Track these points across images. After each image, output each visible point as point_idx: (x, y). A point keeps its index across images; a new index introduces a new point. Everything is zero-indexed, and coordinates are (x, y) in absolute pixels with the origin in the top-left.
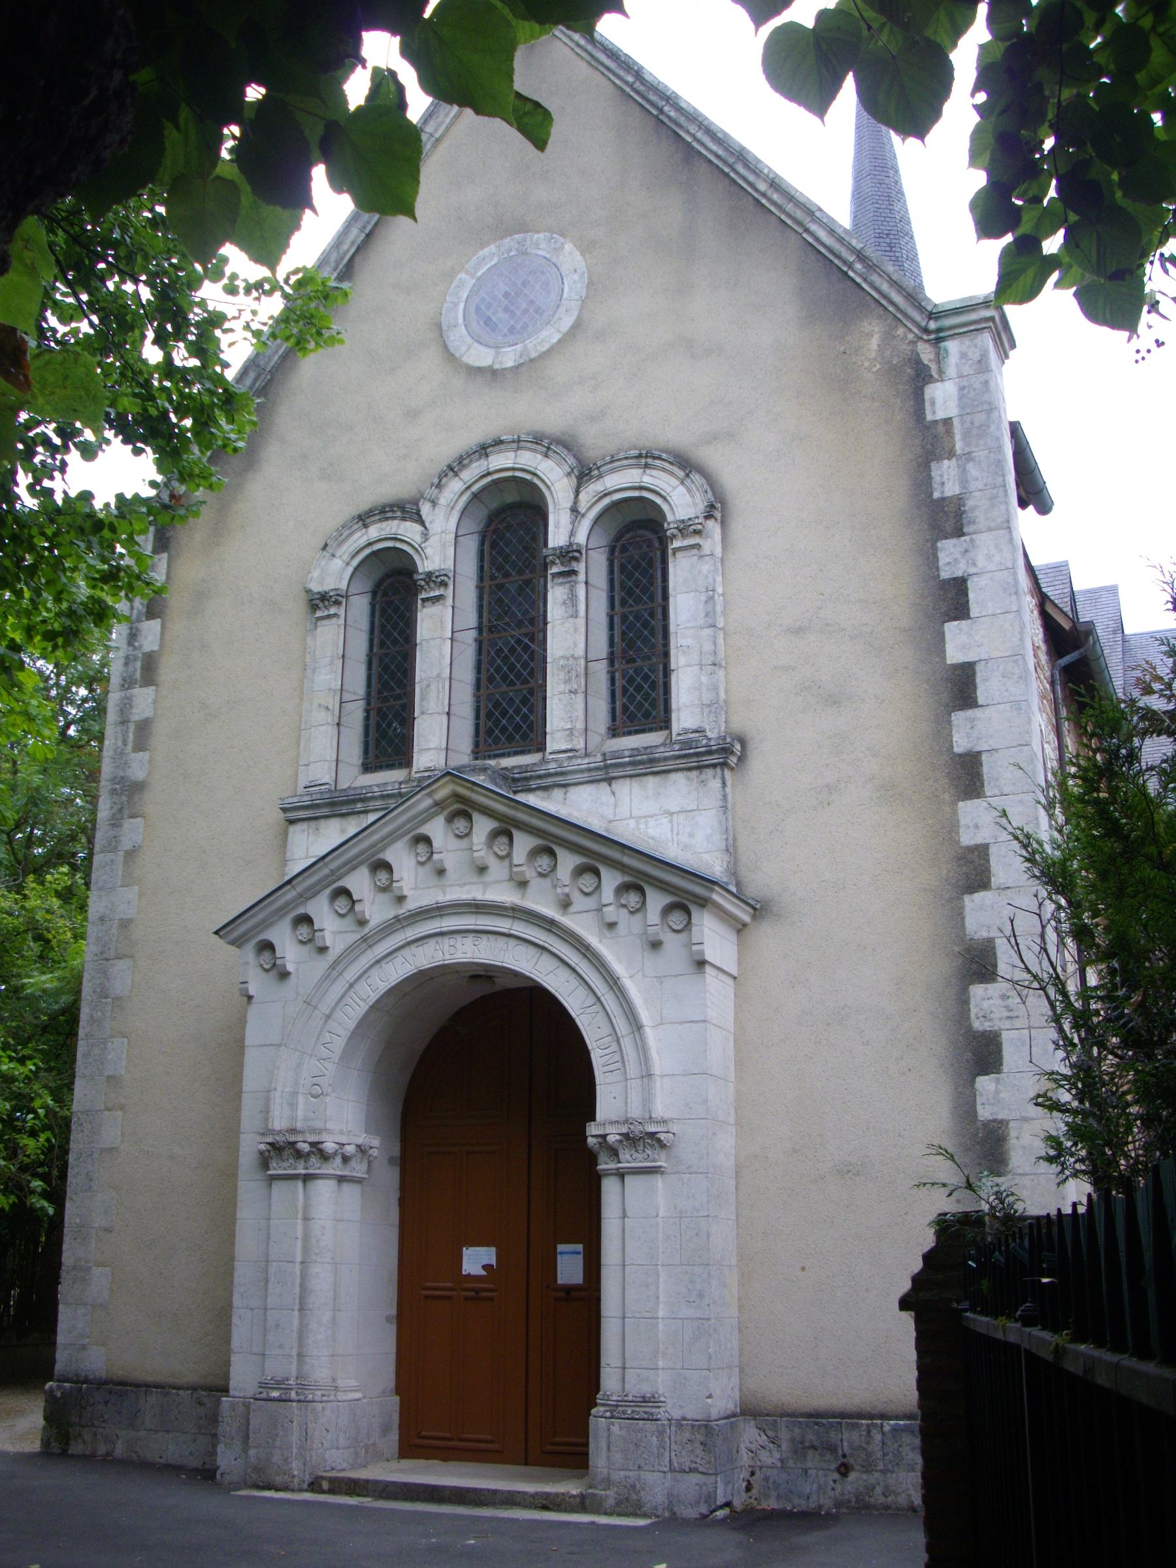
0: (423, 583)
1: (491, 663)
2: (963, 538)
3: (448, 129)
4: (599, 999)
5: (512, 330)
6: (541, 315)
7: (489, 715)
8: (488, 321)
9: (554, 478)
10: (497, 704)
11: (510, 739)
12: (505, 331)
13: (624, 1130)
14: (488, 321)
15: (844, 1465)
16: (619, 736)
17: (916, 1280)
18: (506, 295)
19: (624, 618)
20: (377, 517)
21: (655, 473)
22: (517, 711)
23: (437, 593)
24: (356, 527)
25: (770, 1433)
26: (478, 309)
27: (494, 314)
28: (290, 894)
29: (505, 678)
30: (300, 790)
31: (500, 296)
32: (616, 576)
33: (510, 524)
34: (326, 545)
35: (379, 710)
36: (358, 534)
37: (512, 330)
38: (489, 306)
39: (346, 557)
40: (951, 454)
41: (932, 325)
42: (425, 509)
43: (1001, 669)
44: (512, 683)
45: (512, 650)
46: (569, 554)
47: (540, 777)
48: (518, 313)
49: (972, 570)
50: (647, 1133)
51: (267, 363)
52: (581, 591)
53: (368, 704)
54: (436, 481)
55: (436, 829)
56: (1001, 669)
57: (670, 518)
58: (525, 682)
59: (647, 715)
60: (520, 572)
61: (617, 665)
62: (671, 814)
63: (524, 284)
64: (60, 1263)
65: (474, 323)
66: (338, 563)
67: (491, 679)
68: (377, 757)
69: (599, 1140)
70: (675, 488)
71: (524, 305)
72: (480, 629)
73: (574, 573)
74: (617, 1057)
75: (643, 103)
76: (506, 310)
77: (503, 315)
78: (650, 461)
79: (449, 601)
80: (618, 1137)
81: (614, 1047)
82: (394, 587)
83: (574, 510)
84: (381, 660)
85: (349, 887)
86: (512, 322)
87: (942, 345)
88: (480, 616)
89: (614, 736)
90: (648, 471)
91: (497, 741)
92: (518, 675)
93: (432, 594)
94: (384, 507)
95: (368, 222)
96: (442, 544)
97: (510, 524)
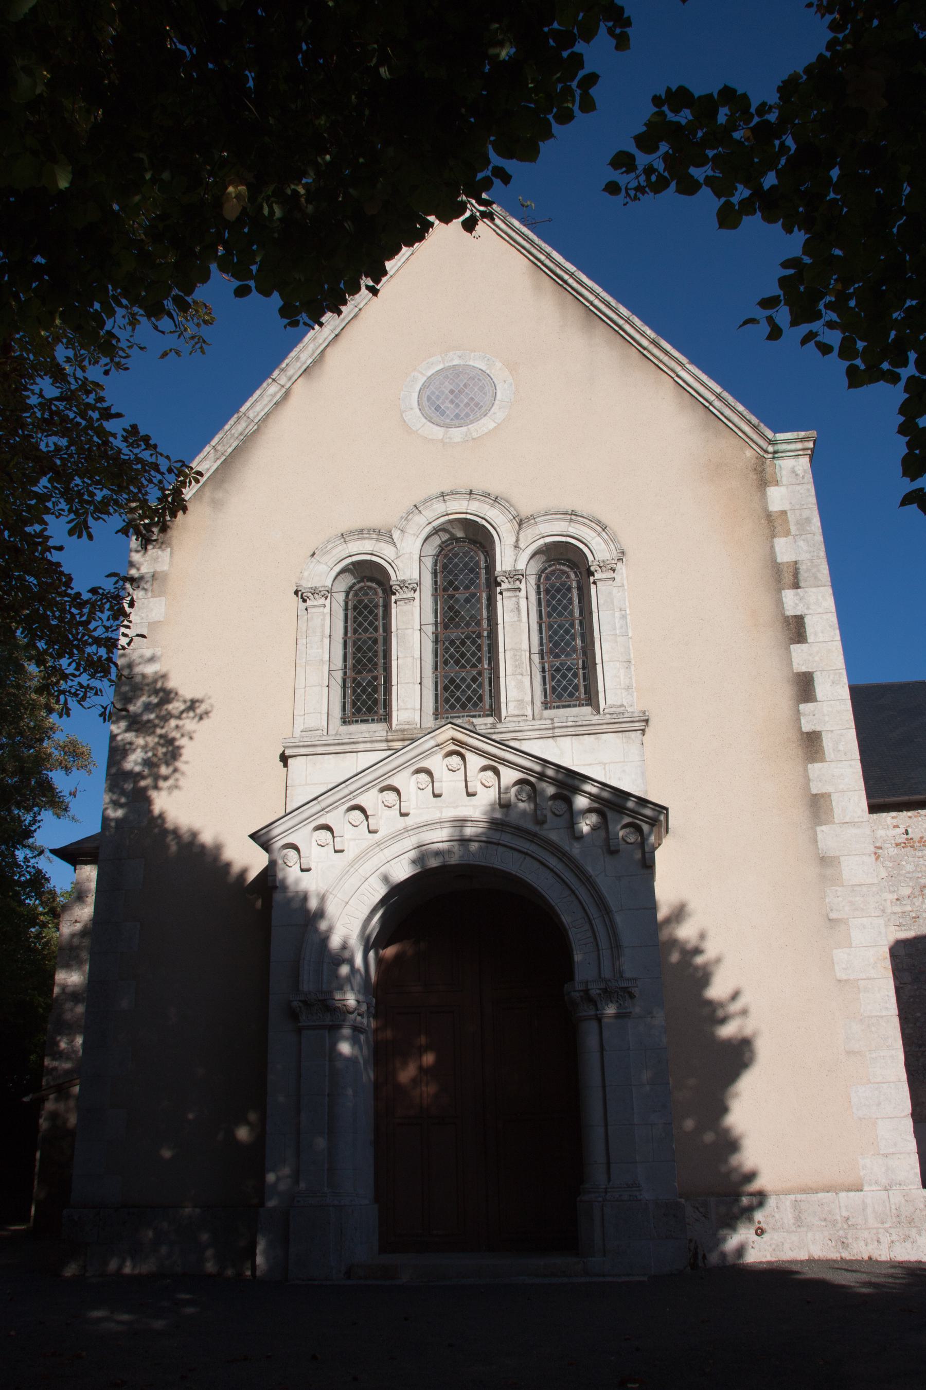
0: (398, 588)
1: (447, 650)
2: (799, 590)
3: (398, 270)
4: (573, 892)
5: (457, 416)
6: (480, 408)
7: (446, 688)
8: (438, 408)
9: (498, 521)
10: (452, 681)
11: (464, 707)
12: (452, 416)
13: (603, 986)
14: (438, 408)
15: (759, 1228)
16: (550, 708)
17: (731, 1145)
18: (452, 392)
19: (550, 627)
20: (356, 537)
21: (577, 526)
22: (469, 687)
23: (409, 596)
24: (339, 542)
25: (701, 1210)
26: (429, 398)
27: (443, 403)
28: (315, 807)
29: (457, 662)
30: (297, 733)
31: (447, 392)
32: (542, 596)
33: (464, 553)
34: (314, 554)
35: (354, 680)
36: (340, 548)
37: (457, 416)
38: (438, 398)
39: (331, 564)
40: (787, 533)
41: (770, 449)
42: (396, 535)
43: (831, 677)
44: (463, 666)
45: (463, 643)
46: (516, 576)
47: (501, 733)
48: (462, 405)
49: (806, 612)
50: (621, 988)
51: (255, 417)
52: (523, 603)
53: (345, 673)
54: (405, 515)
55: (436, 763)
56: (831, 677)
57: (393, 577)
58: (474, 666)
59: (571, 695)
60: (467, 588)
61: (546, 658)
62: (605, 764)
63: (465, 385)
64: (902, 811)
65: (427, 409)
66: (323, 568)
67: (446, 663)
68: (353, 714)
69: (582, 994)
70: (593, 538)
71: (466, 400)
72: (436, 624)
73: (519, 590)
74: (590, 934)
75: (554, 277)
76: (452, 402)
77: (447, 404)
78: (573, 517)
79: (417, 601)
80: (598, 991)
81: (587, 927)
82: (368, 590)
83: (516, 546)
84: (355, 643)
85: (363, 804)
86: (457, 411)
87: (777, 462)
88: (436, 617)
89: (546, 708)
90: (572, 524)
91: (452, 707)
92: (468, 661)
93: (405, 596)
94: (362, 530)
95: (338, 326)
96: (409, 561)
97: (464, 553)
